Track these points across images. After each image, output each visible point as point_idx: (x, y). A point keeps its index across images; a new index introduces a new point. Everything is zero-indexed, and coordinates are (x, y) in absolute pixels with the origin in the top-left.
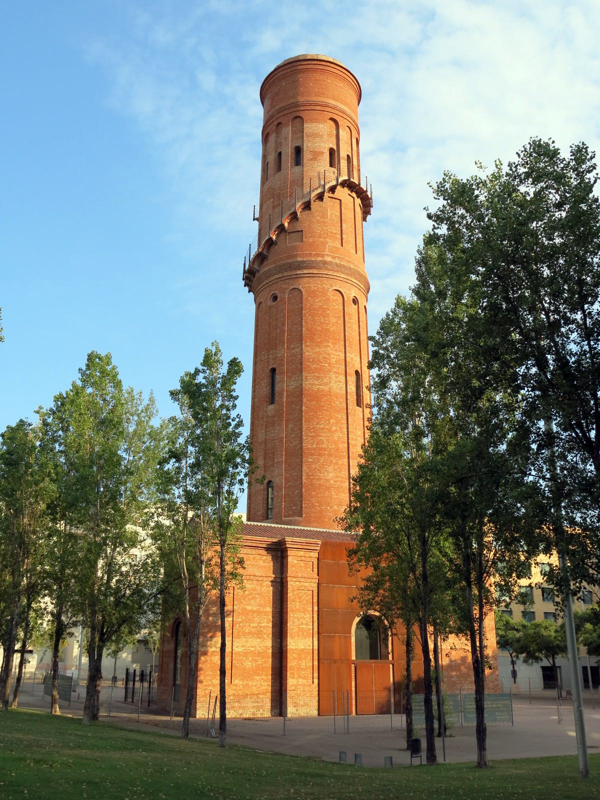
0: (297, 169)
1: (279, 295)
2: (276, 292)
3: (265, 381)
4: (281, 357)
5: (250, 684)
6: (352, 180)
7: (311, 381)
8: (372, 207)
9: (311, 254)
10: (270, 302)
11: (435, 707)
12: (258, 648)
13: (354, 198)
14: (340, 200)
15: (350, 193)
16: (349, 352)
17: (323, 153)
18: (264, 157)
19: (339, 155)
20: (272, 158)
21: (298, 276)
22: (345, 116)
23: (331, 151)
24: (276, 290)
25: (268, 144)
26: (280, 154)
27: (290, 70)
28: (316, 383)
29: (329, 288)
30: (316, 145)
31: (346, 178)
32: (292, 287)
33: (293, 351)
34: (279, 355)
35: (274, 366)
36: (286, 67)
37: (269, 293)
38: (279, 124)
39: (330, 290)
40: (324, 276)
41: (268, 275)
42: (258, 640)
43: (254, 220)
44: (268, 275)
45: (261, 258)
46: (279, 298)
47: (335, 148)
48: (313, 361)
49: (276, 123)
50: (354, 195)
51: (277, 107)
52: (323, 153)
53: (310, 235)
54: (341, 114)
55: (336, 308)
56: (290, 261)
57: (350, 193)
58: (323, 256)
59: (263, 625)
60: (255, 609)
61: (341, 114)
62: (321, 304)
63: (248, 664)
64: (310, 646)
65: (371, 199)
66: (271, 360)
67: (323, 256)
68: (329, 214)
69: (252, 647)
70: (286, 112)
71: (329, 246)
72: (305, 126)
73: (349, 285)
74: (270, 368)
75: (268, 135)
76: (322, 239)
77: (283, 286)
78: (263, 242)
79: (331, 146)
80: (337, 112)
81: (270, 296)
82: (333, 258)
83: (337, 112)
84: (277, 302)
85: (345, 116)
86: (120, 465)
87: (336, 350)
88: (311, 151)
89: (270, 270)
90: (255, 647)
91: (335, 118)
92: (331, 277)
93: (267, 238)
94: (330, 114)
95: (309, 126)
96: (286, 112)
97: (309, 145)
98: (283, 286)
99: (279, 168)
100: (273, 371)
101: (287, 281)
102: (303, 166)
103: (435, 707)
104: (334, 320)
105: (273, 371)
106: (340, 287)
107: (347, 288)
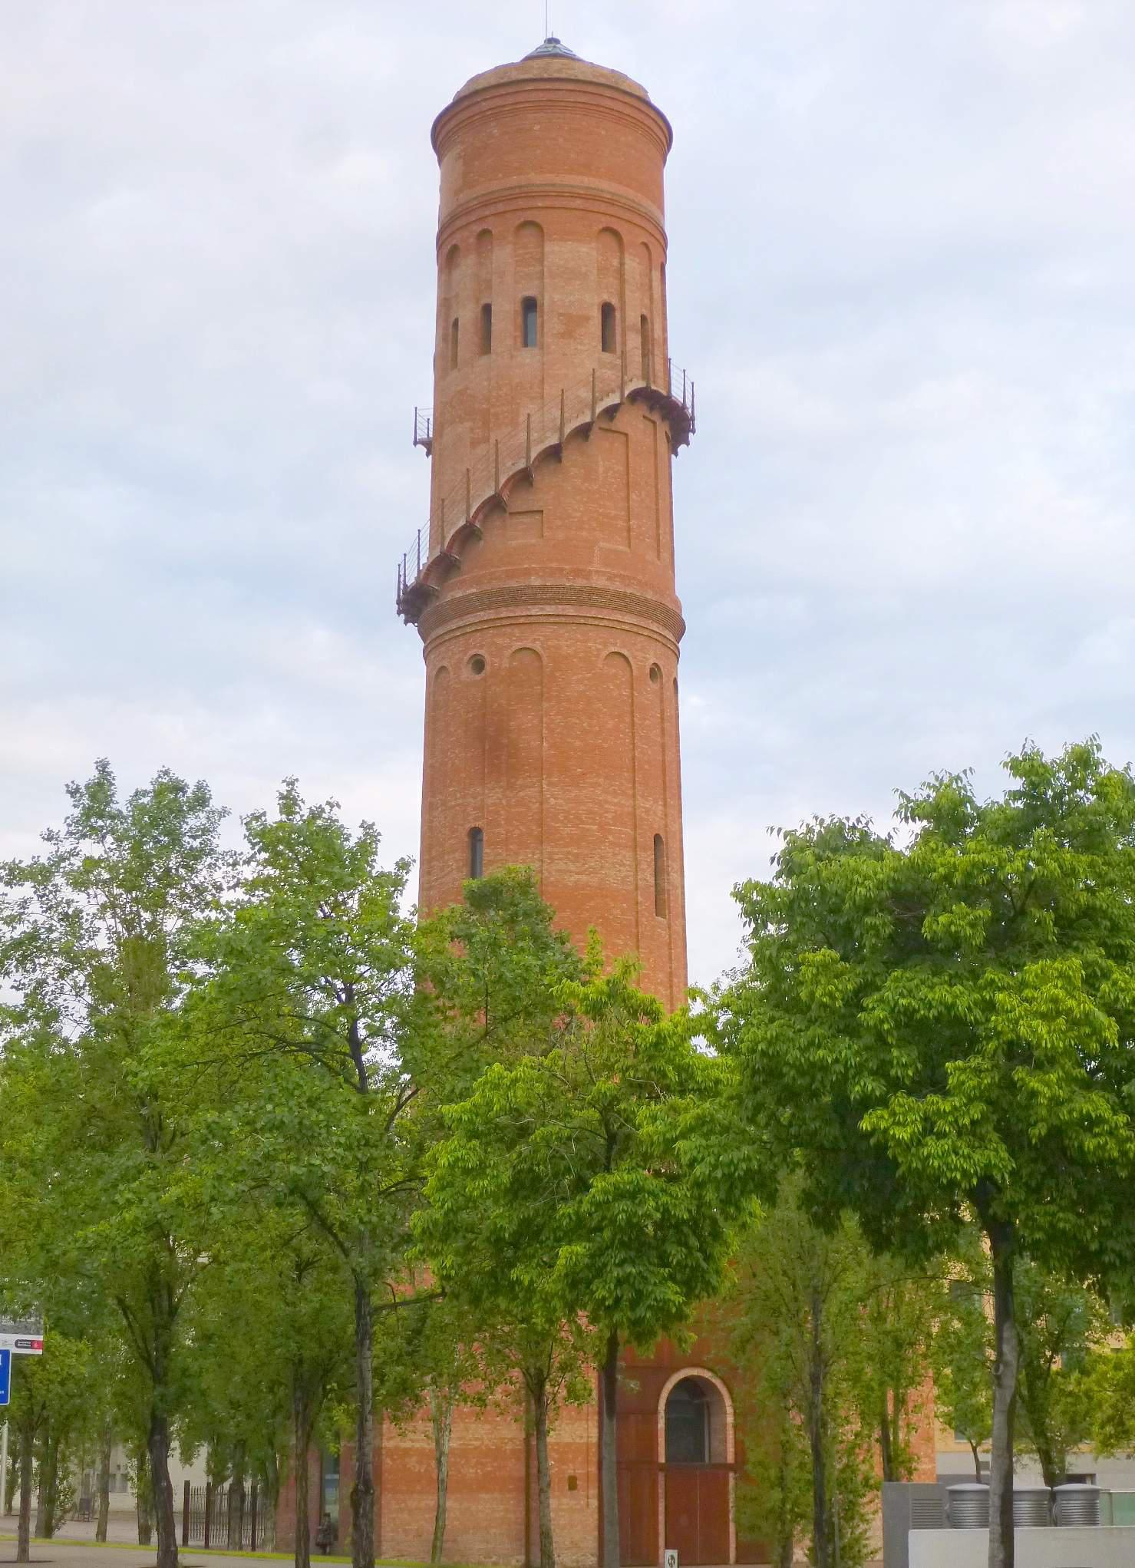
0: (528, 357)
1: (488, 659)
2: (481, 652)
3: (457, 855)
4: (494, 804)
5: (473, 1508)
6: (653, 387)
7: (562, 866)
8: (694, 432)
9: (562, 570)
10: (467, 674)
11: (510, 90)
12: (486, 1442)
13: (654, 423)
14: (626, 435)
15: (647, 414)
16: (643, 796)
17: (587, 319)
18: (445, 305)
19: (623, 320)
20: (468, 314)
21: (532, 620)
22: (637, 220)
23: (607, 310)
24: (482, 647)
25: (457, 274)
26: (487, 309)
27: (510, 100)
28: (572, 867)
29: (598, 650)
30: (572, 298)
31: (641, 384)
32: (518, 645)
33: (522, 794)
34: (490, 801)
35: (478, 824)
36: (502, 91)
37: (465, 652)
38: (486, 232)
39: (604, 653)
40: (591, 621)
41: (462, 607)
42: (487, 1427)
43: (416, 443)
44: (462, 607)
45: (443, 566)
46: (488, 668)
47: (614, 301)
48: (566, 818)
49: (477, 228)
50: (656, 417)
51: (479, 190)
52: (587, 319)
53: (559, 522)
54: (627, 215)
55: (615, 694)
56: (513, 584)
57: (647, 414)
58: (587, 575)
61: (627, 215)
62: (582, 688)
63: (470, 1472)
65: (693, 419)
66: (469, 809)
67: (587, 575)
68: (601, 470)
69: (476, 1439)
70: (501, 207)
71: (601, 549)
72: (547, 249)
73: (642, 638)
74: (468, 826)
75: (455, 249)
76: (584, 534)
77: (499, 641)
78: (452, 532)
79: (605, 297)
80: (621, 213)
81: (466, 658)
82: (609, 579)
83: (621, 213)
84: (483, 674)
85: (637, 220)
86: (403, 1224)
87: (615, 794)
88: (561, 315)
89: (466, 599)
90: (481, 1439)
91: (615, 227)
92: (606, 623)
93: (462, 523)
94: (603, 218)
95: (556, 248)
96: (501, 207)
97: (557, 297)
98: (499, 641)
99: (485, 343)
100: (475, 834)
101: (508, 630)
102: (542, 348)
103: (510, 90)
104: (611, 724)
105: (475, 834)
106: (624, 647)
107: (639, 646)
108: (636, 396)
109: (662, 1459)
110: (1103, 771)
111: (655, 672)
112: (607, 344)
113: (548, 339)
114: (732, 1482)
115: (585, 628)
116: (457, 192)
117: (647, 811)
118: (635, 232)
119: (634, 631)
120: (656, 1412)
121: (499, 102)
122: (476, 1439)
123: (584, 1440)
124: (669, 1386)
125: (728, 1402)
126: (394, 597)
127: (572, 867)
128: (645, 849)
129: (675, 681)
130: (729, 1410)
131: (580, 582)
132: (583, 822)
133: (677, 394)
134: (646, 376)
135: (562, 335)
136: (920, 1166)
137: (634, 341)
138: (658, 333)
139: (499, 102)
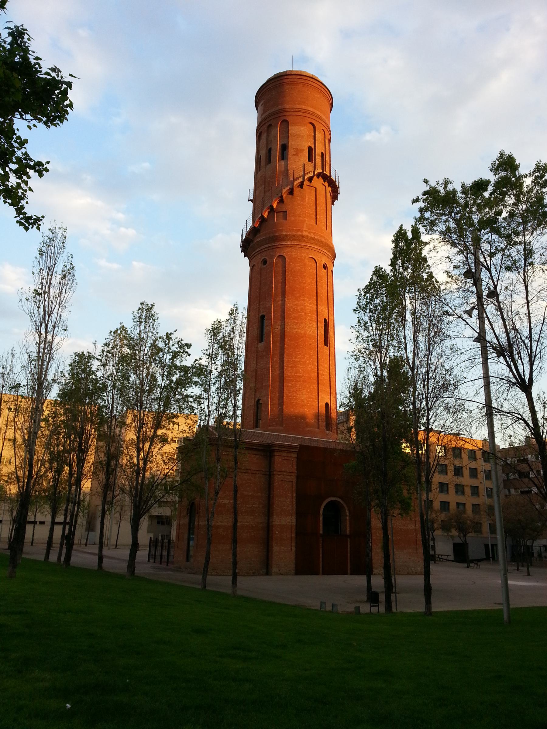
20: (263, 153)
23: (310, 149)
26: (270, 150)
27: (279, 82)
39: (307, 258)
42: (252, 517)
47: (313, 146)
51: (269, 112)
55: (311, 271)
59: (255, 506)
60: (250, 494)
64: (289, 523)
65: (339, 187)
67: (302, 231)
68: (307, 198)
69: (248, 522)
75: (261, 133)
79: (310, 145)
80: (315, 118)
82: (309, 233)
83: (315, 118)
87: (310, 303)
108: (319, 175)
109: (321, 532)
110: (152, 535)
111: (325, 267)
112: (310, 160)
113: (290, 156)
114: (348, 529)
115: (301, 249)
116: (262, 115)
117: (322, 310)
118: (320, 127)
119: (319, 251)
120: (319, 514)
121: (274, 84)
122: (248, 522)
123: (290, 524)
124: (324, 504)
125: (347, 511)
126: (239, 243)
127: (295, 327)
128: (321, 323)
129: (332, 271)
130: (348, 514)
131: (299, 233)
132: (298, 312)
133: (333, 177)
134: (322, 168)
135: (295, 155)
136: (138, 382)
137: (319, 159)
138: (327, 159)
139: (274, 84)
